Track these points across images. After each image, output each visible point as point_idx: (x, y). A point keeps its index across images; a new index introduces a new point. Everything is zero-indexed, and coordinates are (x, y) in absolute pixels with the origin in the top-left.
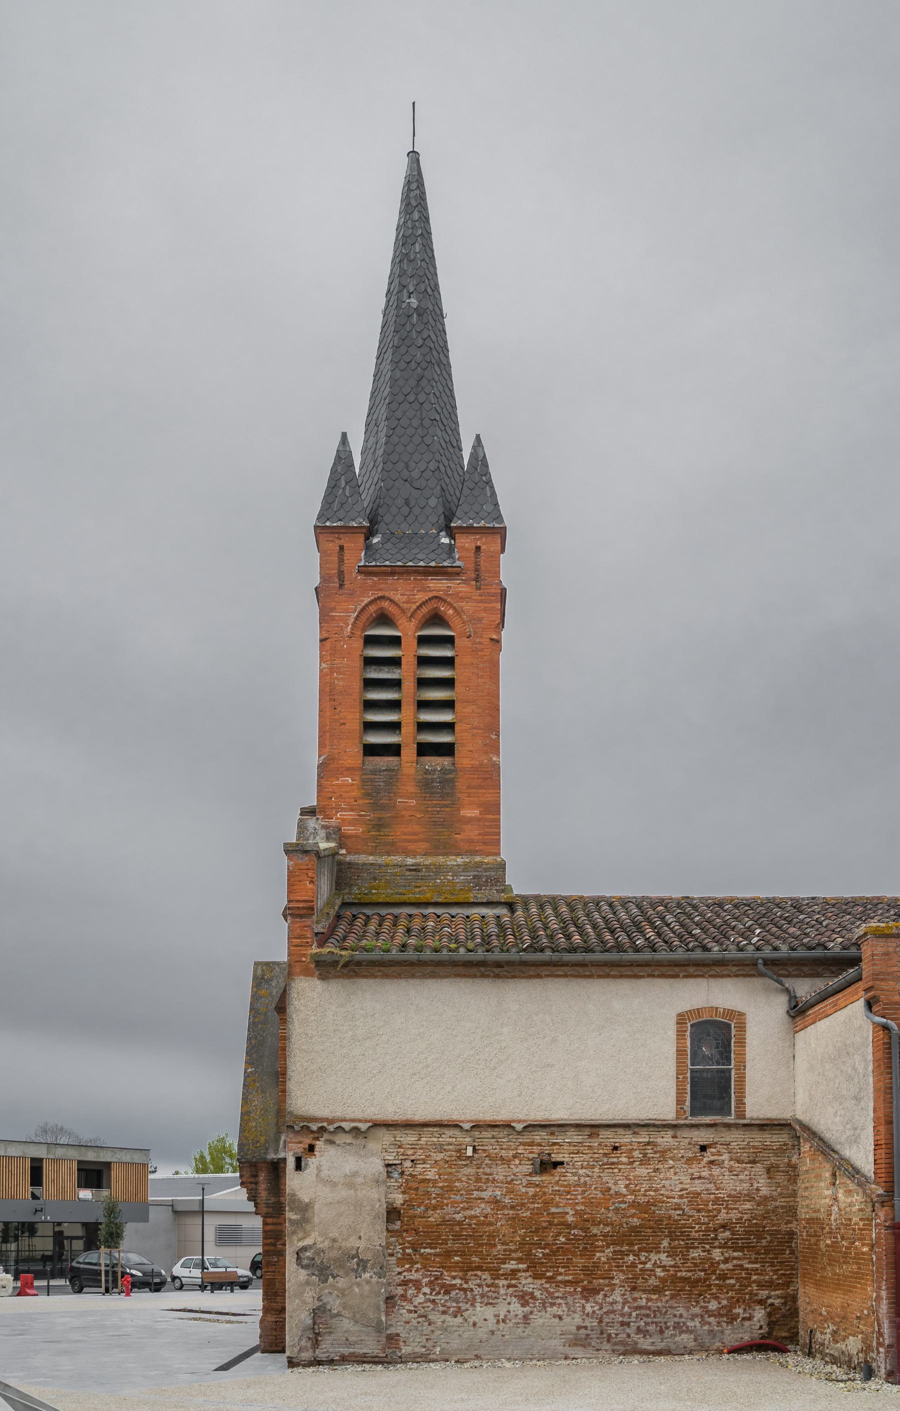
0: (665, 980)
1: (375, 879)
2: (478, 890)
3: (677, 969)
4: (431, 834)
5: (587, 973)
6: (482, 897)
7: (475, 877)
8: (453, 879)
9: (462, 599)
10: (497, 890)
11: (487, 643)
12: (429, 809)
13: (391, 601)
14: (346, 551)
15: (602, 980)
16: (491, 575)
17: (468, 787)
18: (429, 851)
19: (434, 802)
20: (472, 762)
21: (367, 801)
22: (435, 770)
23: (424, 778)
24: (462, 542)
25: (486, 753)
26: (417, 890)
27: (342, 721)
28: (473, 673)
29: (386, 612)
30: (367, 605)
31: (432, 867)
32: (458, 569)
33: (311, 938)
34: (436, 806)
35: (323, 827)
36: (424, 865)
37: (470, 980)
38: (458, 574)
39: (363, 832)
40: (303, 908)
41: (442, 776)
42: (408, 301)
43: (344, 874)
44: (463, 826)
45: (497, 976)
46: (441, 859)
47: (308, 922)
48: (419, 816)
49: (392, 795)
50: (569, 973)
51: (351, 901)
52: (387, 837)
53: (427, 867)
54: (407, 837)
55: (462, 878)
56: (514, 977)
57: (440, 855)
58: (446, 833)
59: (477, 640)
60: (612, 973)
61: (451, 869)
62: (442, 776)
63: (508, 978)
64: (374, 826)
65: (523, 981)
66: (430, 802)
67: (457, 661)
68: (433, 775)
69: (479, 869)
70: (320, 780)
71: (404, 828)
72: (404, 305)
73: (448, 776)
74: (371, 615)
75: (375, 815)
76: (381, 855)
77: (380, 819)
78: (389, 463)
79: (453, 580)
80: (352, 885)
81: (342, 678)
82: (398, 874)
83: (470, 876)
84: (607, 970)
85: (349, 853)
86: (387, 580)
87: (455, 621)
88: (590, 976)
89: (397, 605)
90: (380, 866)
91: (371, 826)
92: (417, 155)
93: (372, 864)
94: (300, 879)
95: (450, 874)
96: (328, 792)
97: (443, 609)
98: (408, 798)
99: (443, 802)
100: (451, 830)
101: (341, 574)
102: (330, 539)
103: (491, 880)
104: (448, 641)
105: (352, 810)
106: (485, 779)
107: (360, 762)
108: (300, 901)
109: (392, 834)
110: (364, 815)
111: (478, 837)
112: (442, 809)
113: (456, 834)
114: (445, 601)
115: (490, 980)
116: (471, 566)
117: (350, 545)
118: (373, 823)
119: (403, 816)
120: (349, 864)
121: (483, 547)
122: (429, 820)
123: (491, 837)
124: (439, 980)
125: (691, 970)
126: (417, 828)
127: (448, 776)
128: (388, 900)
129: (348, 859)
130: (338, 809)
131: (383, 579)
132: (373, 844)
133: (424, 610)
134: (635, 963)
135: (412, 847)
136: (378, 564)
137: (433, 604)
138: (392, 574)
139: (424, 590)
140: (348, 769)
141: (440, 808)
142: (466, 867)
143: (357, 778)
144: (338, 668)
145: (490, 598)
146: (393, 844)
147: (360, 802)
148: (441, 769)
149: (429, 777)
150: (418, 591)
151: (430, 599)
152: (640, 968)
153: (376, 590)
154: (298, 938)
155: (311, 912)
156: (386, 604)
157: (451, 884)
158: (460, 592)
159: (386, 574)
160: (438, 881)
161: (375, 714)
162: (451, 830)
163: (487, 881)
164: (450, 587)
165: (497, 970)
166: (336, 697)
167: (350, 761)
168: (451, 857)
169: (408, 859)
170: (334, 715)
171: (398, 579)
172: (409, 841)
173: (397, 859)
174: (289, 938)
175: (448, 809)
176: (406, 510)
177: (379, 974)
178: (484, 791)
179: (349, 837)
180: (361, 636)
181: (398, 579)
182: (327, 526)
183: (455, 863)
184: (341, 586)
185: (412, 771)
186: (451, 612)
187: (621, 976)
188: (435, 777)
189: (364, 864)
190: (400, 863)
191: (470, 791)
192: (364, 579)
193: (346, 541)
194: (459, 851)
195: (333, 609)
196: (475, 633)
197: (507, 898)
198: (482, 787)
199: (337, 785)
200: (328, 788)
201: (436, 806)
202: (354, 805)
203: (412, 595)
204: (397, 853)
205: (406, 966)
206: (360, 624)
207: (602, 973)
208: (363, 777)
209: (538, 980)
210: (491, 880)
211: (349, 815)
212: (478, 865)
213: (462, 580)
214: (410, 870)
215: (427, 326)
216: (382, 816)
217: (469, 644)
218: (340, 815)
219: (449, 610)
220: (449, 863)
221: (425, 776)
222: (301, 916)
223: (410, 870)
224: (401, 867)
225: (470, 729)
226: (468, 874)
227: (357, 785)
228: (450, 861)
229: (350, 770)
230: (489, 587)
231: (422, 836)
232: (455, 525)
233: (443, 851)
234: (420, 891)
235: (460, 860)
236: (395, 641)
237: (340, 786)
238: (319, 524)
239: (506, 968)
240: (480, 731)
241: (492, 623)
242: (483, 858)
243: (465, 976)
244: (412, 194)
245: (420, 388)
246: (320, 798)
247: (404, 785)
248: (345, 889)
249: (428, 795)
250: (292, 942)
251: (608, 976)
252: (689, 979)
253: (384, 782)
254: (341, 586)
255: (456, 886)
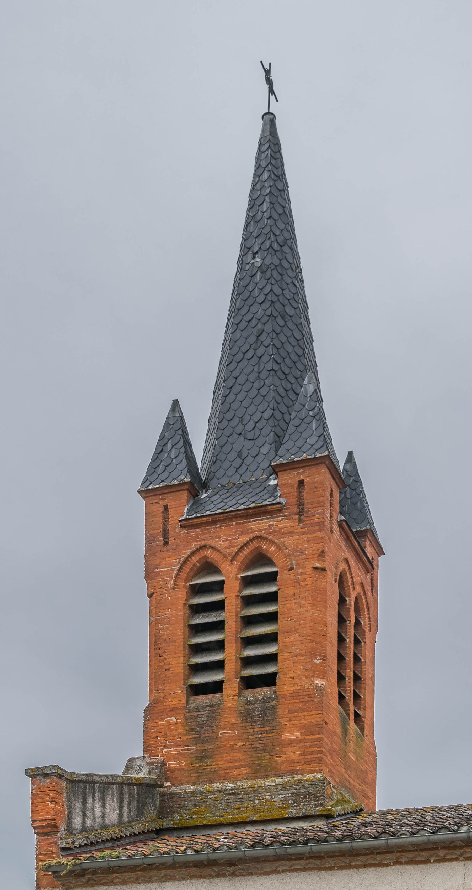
0: (415, 866)
1: (196, 805)
2: (296, 806)
3: (425, 854)
4: (252, 759)
5: (327, 865)
6: (296, 812)
7: (293, 794)
8: (272, 798)
9: (284, 534)
10: (315, 805)
11: (310, 572)
12: (250, 737)
13: (213, 548)
14: (170, 510)
15: (344, 871)
16: (314, 506)
17: (290, 712)
18: (249, 775)
19: (255, 730)
20: (293, 688)
21: (191, 737)
22: (256, 701)
23: (245, 709)
24: (285, 480)
25: (307, 677)
26: (236, 812)
27: (166, 667)
28: (295, 603)
29: (209, 560)
30: (189, 556)
31: (251, 789)
32: (278, 506)
33: (57, 853)
34: (257, 733)
35: (149, 764)
36: (243, 788)
37: (207, 881)
38: (280, 511)
39: (187, 764)
40: (47, 826)
41: (263, 704)
42: (252, 261)
43: (167, 804)
44: (284, 749)
45: (233, 875)
46: (261, 781)
47: (53, 838)
48: (240, 744)
49: (214, 728)
50: (308, 866)
51: (170, 826)
52: (209, 767)
53: (246, 790)
54: (229, 765)
55: (281, 796)
56: (251, 874)
57: (261, 778)
58: (267, 757)
59: (300, 571)
60: (354, 863)
61: (269, 789)
62: (263, 704)
63: (245, 876)
64: (197, 758)
65: (261, 877)
66: (251, 731)
67: (279, 595)
68: (254, 705)
69: (298, 787)
70: (147, 722)
71: (227, 756)
72: (248, 267)
73: (269, 704)
74: (195, 565)
75: (199, 748)
76: (203, 783)
77: (203, 751)
78: (224, 420)
79: (275, 517)
80: (174, 812)
81: (167, 628)
82: (218, 799)
83: (288, 794)
84: (347, 861)
85: (173, 785)
86: (209, 529)
87: (277, 558)
88: (331, 868)
89: (218, 551)
90: (201, 793)
91: (194, 759)
92: (271, 117)
93: (193, 792)
94: (42, 800)
95: (268, 794)
96: (154, 732)
97: (265, 547)
98: (231, 729)
99: (265, 729)
100: (271, 754)
101: (165, 533)
102: (156, 501)
103: (309, 796)
104: (272, 577)
105: (176, 746)
106: (306, 702)
107: (184, 701)
108: (43, 820)
109: (215, 763)
110: (188, 750)
111: (299, 758)
112: (263, 735)
113: (277, 757)
114: (266, 539)
115: (227, 879)
116: (294, 501)
117: (173, 503)
118: (197, 755)
119: (225, 746)
120: (172, 794)
121: (307, 480)
122: (250, 746)
123: (312, 756)
124: (177, 883)
125: (442, 853)
126: (239, 756)
127: (269, 704)
128: (205, 823)
129: (171, 790)
130: (164, 746)
131: (205, 530)
132: (196, 775)
133: (246, 551)
134: (376, 851)
135: (233, 773)
136: (198, 515)
137: (255, 544)
138: (214, 522)
139: (245, 532)
140: (172, 710)
141: (261, 734)
142: (284, 787)
143: (182, 717)
144: (163, 619)
145: (313, 528)
146: (215, 773)
147: (185, 738)
148: (263, 699)
149: (251, 707)
150: (240, 535)
151: (251, 540)
152: (383, 856)
153: (199, 541)
154: (46, 854)
155: (55, 830)
156: (208, 553)
157: (269, 803)
158: (282, 528)
159: (208, 524)
160: (257, 801)
161: (202, 657)
162: (271, 754)
163: (305, 797)
164: (272, 525)
165: (231, 869)
166: (160, 646)
167: (174, 702)
168: (271, 779)
169: (229, 785)
170: (160, 663)
171: (221, 526)
172: (231, 768)
173: (217, 786)
174: (37, 855)
175: (269, 735)
176: (239, 461)
177: (118, 880)
178: (305, 714)
179: (173, 770)
180: (184, 587)
181: (221, 526)
182: (149, 489)
183: (274, 784)
184: (166, 543)
185: (234, 704)
186: (273, 548)
187: (364, 866)
188: (256, 706)
189: (186, 793)
190: (219, 789)
191: (292, 715)
192: (188, 533)
193: (170, 501)
194: (280, 773)
195: (158, 566)
196: (298, 564)
197: (323, 810)
198: (304, 710)
199: (162, 725)
200: (153, 729)
201: (257, 733)
202: (178, 741)
203: (234, 539)
204: (219, 780)
205: (139, 871)
206: (183, 575)
207: (343, 864)
208: (187, 715)
209: (277, 875)
210: (309, 796)
211: (174, 751)
212: (296, 783)
213: (285, 516)
214: (230, 794)
215: (269, 281)
216: (205, 748)
217: (292, 577)
218: (165, 752)
219: (271, 547)
220: (267, 784)
221: (246, 707)
222: (47, 834)
223: (230, 794)
224: (220, 792)
225: (292, 657)
226: (287, 792)
227: (181, 723)
228: (269, 782)
229: (174, 710)
230: (312, 518)
231: (244, 763)
232: (275, 463)
233: (263, 774)
234: (239, 813)
235: (278, 781)
236: (219, 586)
237: (165, 726)
238: (364, 543)
239: (239, 866)
240: (302, 658)
241: (315, 552)
242: (303, 777)
243: (200, 877)
244: (263, 156)
245: (260, 343)
246: (147, 739)
247: (226, 717)
248: (168, 817)
249: (250, 724)
250: (39, 858)
251: (349, 866)
252: (442, 864)
253: (206, 717)
254: (166, 543)
255: (274, 804)
